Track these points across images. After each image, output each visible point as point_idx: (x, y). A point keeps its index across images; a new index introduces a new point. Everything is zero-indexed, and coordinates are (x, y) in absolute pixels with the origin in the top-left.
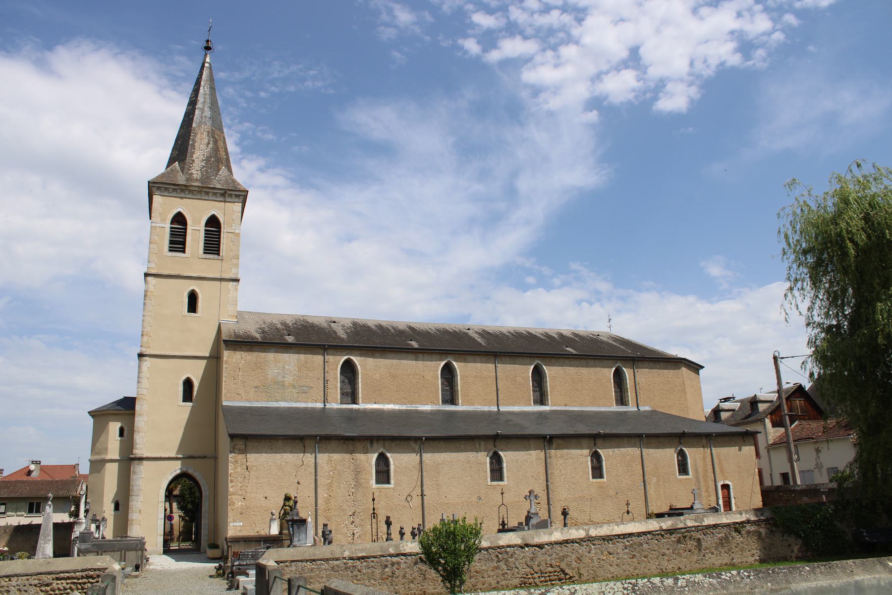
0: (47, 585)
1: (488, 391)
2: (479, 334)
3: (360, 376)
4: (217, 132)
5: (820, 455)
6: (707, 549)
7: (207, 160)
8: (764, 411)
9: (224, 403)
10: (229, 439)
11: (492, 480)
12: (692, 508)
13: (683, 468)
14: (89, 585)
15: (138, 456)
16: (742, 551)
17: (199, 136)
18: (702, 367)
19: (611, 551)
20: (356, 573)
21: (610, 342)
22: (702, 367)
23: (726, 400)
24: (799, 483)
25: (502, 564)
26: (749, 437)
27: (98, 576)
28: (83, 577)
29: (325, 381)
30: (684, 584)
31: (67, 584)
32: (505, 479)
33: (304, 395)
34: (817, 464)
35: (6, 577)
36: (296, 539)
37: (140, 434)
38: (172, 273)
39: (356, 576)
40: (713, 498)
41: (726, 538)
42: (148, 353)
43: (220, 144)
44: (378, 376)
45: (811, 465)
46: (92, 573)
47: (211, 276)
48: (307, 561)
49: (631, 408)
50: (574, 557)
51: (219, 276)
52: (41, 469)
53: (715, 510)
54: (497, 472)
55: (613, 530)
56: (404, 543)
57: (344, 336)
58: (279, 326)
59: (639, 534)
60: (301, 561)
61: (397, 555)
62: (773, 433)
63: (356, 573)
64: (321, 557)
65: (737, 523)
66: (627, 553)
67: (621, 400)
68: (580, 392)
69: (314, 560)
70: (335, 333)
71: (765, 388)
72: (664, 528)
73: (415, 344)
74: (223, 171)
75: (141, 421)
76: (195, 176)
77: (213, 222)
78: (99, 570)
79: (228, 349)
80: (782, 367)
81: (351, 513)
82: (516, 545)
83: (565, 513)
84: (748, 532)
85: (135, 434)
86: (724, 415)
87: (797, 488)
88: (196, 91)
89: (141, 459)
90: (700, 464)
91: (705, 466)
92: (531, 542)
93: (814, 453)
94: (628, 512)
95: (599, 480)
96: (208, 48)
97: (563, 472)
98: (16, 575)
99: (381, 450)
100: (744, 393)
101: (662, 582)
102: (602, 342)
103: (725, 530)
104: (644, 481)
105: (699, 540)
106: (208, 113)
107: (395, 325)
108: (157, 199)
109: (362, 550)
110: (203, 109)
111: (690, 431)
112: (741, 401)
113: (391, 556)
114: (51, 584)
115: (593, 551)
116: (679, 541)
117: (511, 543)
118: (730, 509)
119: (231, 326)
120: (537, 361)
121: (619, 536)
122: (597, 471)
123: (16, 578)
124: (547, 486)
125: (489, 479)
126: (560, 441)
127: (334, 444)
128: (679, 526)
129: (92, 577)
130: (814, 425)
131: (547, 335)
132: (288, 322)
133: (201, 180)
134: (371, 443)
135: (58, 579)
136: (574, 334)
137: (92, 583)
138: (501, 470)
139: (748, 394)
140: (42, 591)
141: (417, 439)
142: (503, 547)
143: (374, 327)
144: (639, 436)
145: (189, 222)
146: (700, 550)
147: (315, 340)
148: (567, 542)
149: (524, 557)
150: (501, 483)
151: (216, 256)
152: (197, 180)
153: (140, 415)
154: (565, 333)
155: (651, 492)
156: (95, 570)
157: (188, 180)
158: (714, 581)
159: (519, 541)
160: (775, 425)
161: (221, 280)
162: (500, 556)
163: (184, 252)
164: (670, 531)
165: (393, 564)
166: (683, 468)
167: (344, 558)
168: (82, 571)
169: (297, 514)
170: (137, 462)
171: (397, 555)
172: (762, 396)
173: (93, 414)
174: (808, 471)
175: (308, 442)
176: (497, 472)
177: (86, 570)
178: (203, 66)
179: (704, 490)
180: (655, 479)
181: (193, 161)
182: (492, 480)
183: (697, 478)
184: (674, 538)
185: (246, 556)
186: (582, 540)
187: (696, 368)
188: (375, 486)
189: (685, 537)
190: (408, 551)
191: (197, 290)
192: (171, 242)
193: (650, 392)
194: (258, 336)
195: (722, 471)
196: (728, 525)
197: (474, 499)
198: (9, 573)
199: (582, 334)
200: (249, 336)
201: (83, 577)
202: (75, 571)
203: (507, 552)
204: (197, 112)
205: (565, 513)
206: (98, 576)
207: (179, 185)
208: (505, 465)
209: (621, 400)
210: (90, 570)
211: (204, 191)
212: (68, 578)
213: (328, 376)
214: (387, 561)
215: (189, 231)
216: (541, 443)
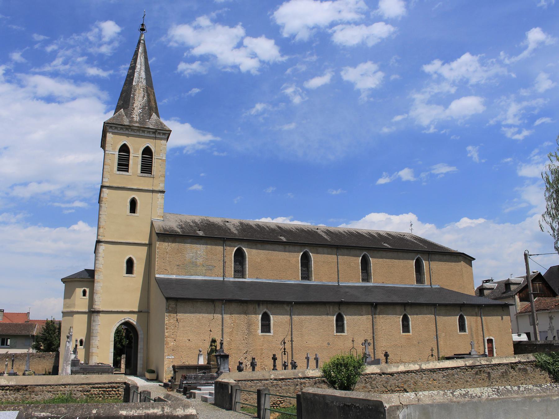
0: (87, 391)
1: (331, 271)
2: (325, 232)
3: (247, 260)
4: (149, 89)
5: (553, 321)
6: (494, 379)
7: (143, 108)
8: (515, 291)
9: (157, 276)
10: (165, 300)
11: (403, 332)
12: (470, 354)
13: (462, 328)
14: (113, 392)
15: (97, 310)
16: (515, 380)
17: (137, 91)
18: (474, 259)
19: (435, 378)
20: (278, 388)
21: (413, 240)
22: (474, 259)
23: (487, 281)
24: (539, 339)
25: (368, 385)
26: (504, 308)
27: (119, 387)
28: (109, 388)
29: (224, 262)
30: (523, 390)
31: (100, 391)
32: (346, 331)
33: (210, 272)
34: (550, 327)
35: (63, 385)
36: (222, 368)
37: (98, 295)
38: (120, 186)
39: (278, 391)
40: (482, 348)
41: (506, 372)
42: (103, 240)
43: (152, 97)
44: (259, 260)
45: (546, 328)
46: (115, 385)
47: (146, 188)
48: (248, 381)
49: (427, 285)
50: (412, 381)
51: (151, 189)
52: (4, 315)
53: (484, 355)
54: (340, 327)
55: (436, 365)
56: (308, 370)
57: (236, 232)
58: (192, 224)
59: (452, 368)
60: (245, 381)
61: (304, 378)
62: (519, 305)
63: (278, 388)
64: (257, 378)
65: (512, 363)
66: (444, 380)
67: (420, 280)
68: (392, 274)
69: (252, 380)
70: (230, 230)
71: (517, 275)
72: (468, 365)
73: (283, 239)
74: (154, 116)
75: (98, 286)
76: (135, 119)
77: (147, 152)
78: (119, 383)
79: (159, 240)
80: (529, 260)
81: (244, 352)
82: (377, 373)
83: (386, 355)
84: (520, 369)
85: (95, 295)
86: (486, 292)
87: (538, 343)
88: (135, 60)
89: (98, 312)
90: (473, 324)
91: (477, 326)
92: (386, 372)
93: (549, 320)
94: (432, 355)
95: (406, 334)
96: (143, 30)
97: (384, 328)
98: (69, 384)
99: (265, 310)
100: (502, 277)
101: (512, 388)
102: (407, 240)
103: (505, 367)
104: (437, 335)
105: (489, 373)
106: (143, 74)
107: (268, 225)
108: (109, 136)
109: (282, 375)
110: (140, 72)
111: (468, 303)
112: (498, 283)
113: (300, 378)
114: (90, 391)
115: (424, 378)
116: (476, 374)
117: (374, 372)
118: (493, 356)
119: (159, 224)
120: (365, 253)
121: (440, 369)
122: (406, 328)
123: (68, 386)
124: (373, 336)
125: (335, 331)
126: (382, 307)
127: (234, 306)
128: (477, 364)
129: (114, 387)
130: (548, 300)
131: (370, 234)
132: (196, 221)
133: (139, 122)
134: (259, 305)
135: (93, 388)
136: (388, 234)
137: (115, 391)
138: (269, 325)
139: (504, 278)
140: (84, 395)
141: (289, 303)
142: (369, 374)
143: (254, 226)
144: (434, 305)
145: (131, 151)
146: (489, 379)
147: (216, 234)
148: (408, 372)
149: (382, 381)
150: (343, 334)
151: (149, 175)
152: (137, 122)
153: (98, 282)
154: (381, 233)
155: (441, 343)
156: (116, 383)
157: (130, 122)
158: (539, 389)
159: (379, 371)
160: (521, 300)
161: (153, 191)
162: (367, 380)
163: (128, 171)
164: (472, 367)
165: (301, 384)
166: (462, 328)
167: (271, 379)
168: (109, 383)
169: (223, 352)
170: (95, 314)
171: (304, 378)
172: (513, 279)
173: (64, 280)
174: (544, 332)
175: (217, 304)
176: (340, 327)
177: (111, 383)
178: (139, 42)
179: (475, 342)
180: (443, 334)
181: (134, 108)
182: (403, 332)
183: (472, 335)
184: (473, 371)
185: (191, 378)
186: (417, 371)
187: (468, 260)
188: (260, 334)
189: (480, 371)
190: (310, 375)
191: (137, 198)
192: (119, 164)
193: (439, 275)
194: (179, 230)
195: (488, 330)
196: (507, 364)
197: (325, 344)
198: (64, 383)
199: (393, 234)
200: (173, 231)
201: (109, 388)
202: (104, 383)
203: (371, 378)
204: (136, 75)
205: (386, 355)
206: (119, 387)
207: (124, 125)
208: (345, 322)
209: (420, 280)
210: (113, 383)
211: (141, 131)
212: (100, 387)
213: (226, 260)
214: (298, 382)
215: (131, 157)
216: (369, 308)
